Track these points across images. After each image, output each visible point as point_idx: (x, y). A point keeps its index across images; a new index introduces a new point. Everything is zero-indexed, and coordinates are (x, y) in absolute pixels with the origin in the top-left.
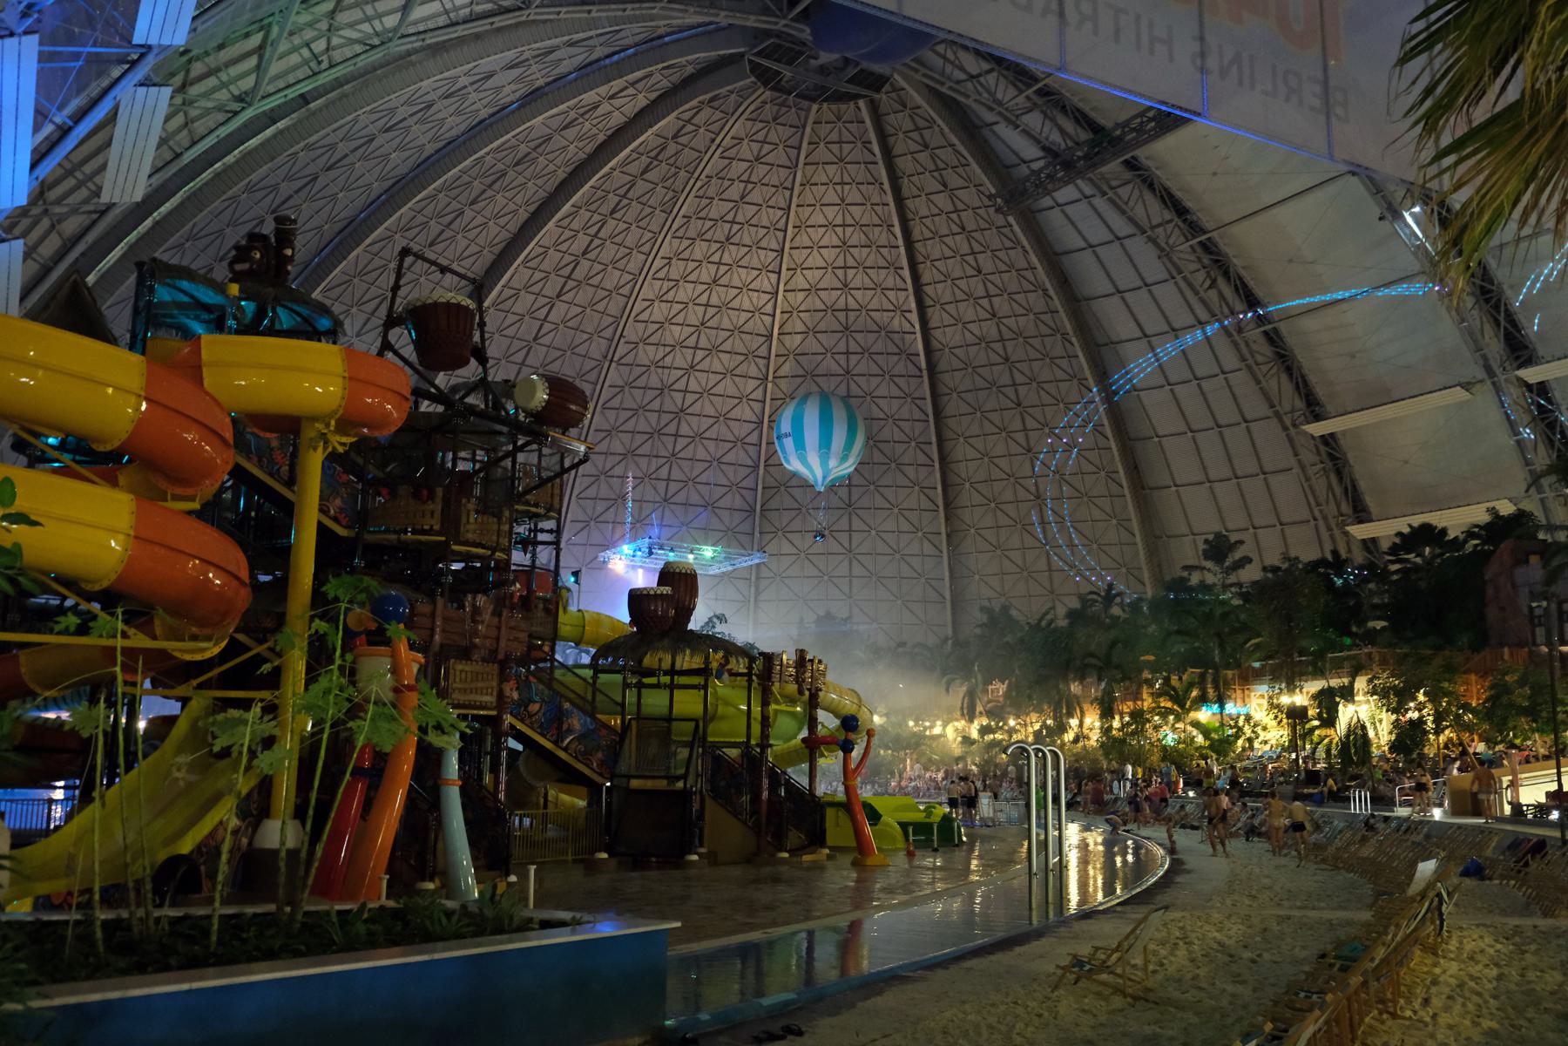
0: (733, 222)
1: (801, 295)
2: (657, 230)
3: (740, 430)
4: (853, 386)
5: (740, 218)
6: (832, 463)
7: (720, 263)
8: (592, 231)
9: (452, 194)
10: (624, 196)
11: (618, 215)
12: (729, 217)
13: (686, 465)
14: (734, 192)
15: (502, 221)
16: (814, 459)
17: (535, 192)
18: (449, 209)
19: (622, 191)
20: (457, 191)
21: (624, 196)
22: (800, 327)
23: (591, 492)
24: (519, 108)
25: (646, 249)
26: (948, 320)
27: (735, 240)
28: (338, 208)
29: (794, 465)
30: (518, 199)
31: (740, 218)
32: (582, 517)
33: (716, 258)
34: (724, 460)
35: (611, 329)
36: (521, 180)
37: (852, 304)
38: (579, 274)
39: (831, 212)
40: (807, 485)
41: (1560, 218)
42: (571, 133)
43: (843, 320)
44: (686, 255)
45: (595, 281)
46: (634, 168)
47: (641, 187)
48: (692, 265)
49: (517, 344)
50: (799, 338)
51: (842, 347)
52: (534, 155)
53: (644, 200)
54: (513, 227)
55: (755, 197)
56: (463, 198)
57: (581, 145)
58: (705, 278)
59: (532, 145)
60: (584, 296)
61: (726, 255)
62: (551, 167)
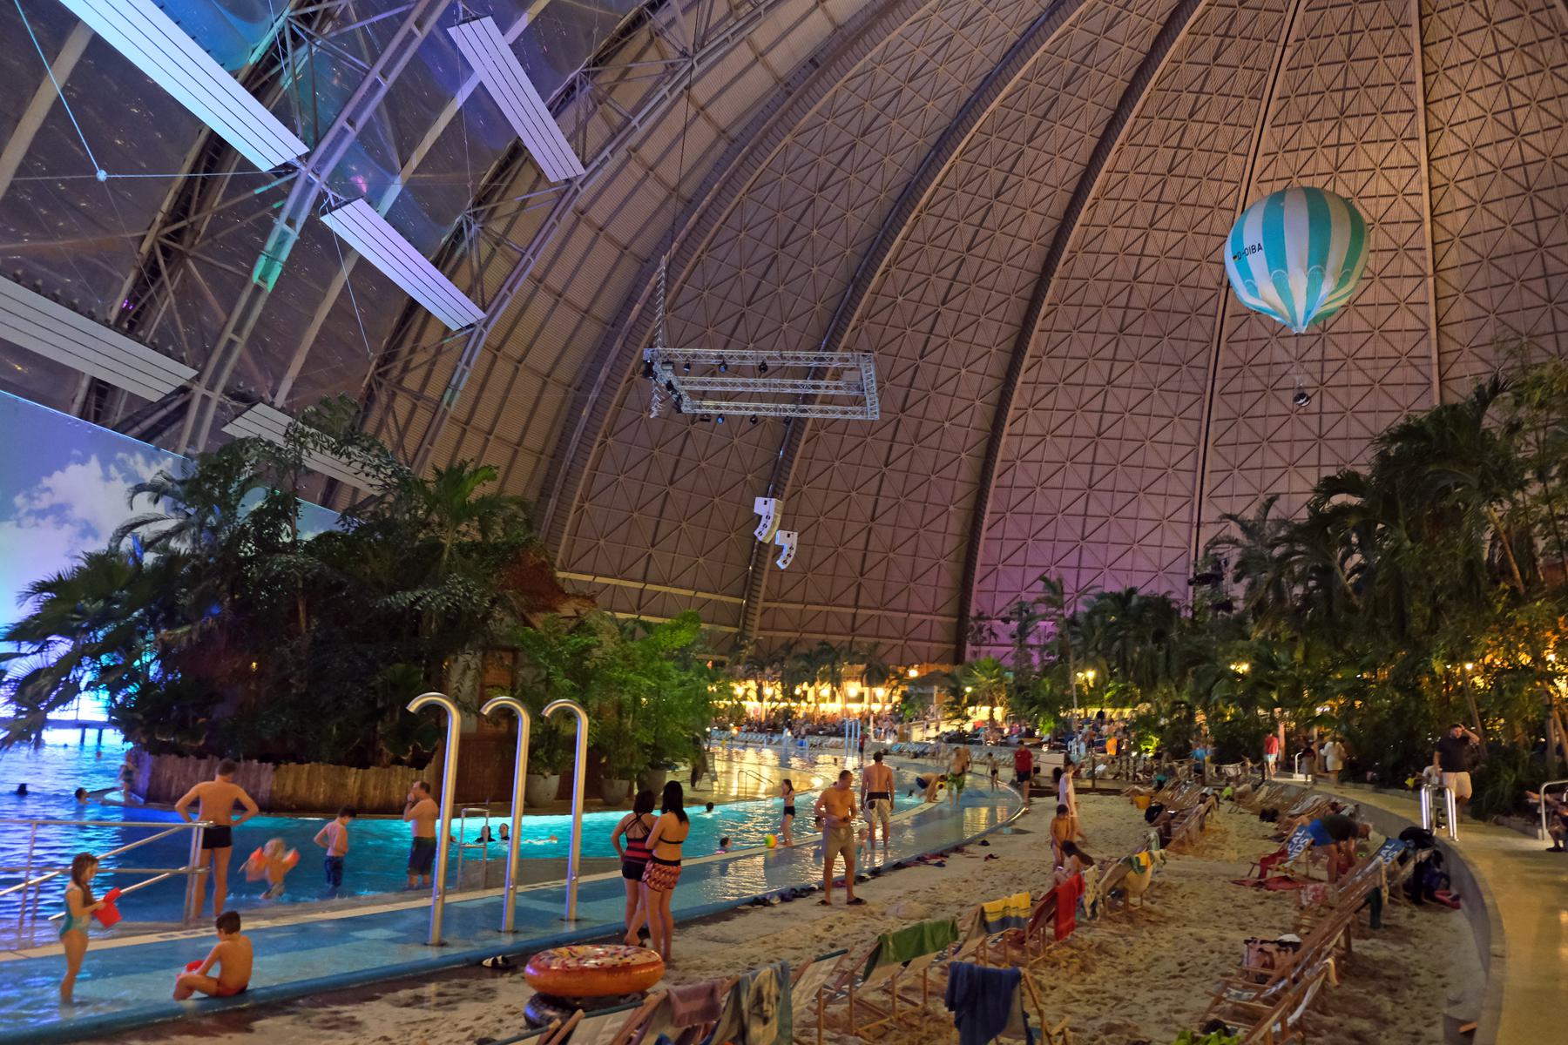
0: (1345, 89)
1: (1456, 160)
2: (1249, 122)
3: (1402, 343)
4: (1550, 261)
5: (1352, 81)
6: (1327, 287)
7: (1339, 145)
8: (1174, 141)
9: (1005, 134)
10: (1201, 91)
11: (1199, 116)
12: (1339, 84)
13: (1340, 394)
14: (1337, 51)
15: (1069, 154)
16: (1298, 282)
17: (1095, 116)
18: (1006, 153)
19: (1196, 87)
20: (1010, 130)
21: (1201, 91)
22: (1462, 202)
23: (1236, 385)
24: (1047, 19)
25: (1242, 148)
26: (1462, 202)
27: (1352, 111)
28: (889, 175)
29: (1250, 300)
30: (1080, 125)
31: (1352, 81)
32: (1222, 465)
33: (1332, 139)
34: (1387, 327)
35: (1203, 356)
36: (1077, 102)
37: (1530, 154)
38: (1169, 195)
39: (1474, 41)
40: (1280, 332)
41: (1356, 1035)
42: (1118, 32)
43: (1532, 235)
44: (1293, 144)
45: (1190, 199)
46: (1204, 54)
47: (1219, 74)
48: (1305, 155)
49: (1175, 125)
50: (1462, 216)
51: (1502, 103)
52: (1083, 69)
53: (1225, 90)
54: (1084, 158)
55: (1365, 48)
56: (1018, 137)
57: (1134, 43)
58: (1107, 326)
59: (1078, 57)
60: (1179, 219)
61: (1345, 132)
62: (1107, 79)
